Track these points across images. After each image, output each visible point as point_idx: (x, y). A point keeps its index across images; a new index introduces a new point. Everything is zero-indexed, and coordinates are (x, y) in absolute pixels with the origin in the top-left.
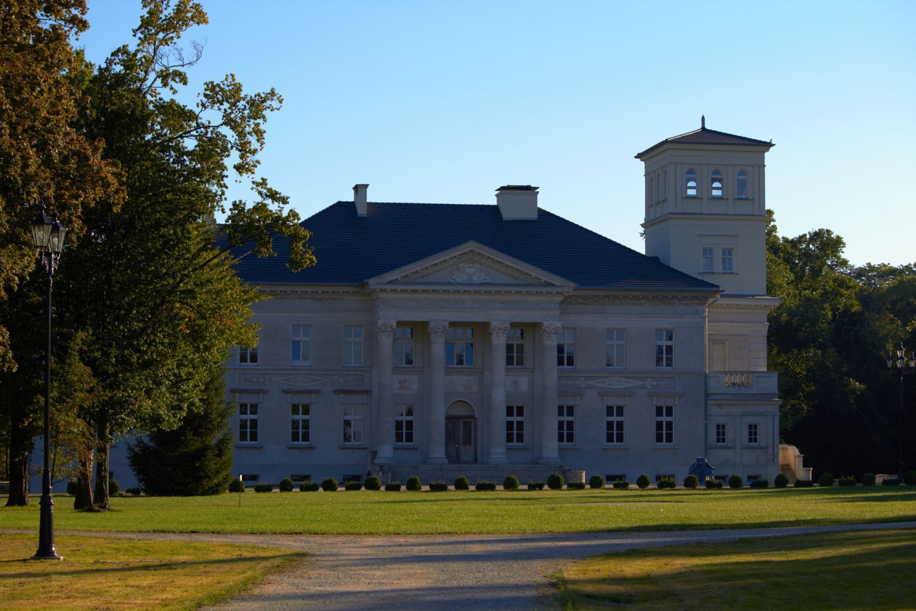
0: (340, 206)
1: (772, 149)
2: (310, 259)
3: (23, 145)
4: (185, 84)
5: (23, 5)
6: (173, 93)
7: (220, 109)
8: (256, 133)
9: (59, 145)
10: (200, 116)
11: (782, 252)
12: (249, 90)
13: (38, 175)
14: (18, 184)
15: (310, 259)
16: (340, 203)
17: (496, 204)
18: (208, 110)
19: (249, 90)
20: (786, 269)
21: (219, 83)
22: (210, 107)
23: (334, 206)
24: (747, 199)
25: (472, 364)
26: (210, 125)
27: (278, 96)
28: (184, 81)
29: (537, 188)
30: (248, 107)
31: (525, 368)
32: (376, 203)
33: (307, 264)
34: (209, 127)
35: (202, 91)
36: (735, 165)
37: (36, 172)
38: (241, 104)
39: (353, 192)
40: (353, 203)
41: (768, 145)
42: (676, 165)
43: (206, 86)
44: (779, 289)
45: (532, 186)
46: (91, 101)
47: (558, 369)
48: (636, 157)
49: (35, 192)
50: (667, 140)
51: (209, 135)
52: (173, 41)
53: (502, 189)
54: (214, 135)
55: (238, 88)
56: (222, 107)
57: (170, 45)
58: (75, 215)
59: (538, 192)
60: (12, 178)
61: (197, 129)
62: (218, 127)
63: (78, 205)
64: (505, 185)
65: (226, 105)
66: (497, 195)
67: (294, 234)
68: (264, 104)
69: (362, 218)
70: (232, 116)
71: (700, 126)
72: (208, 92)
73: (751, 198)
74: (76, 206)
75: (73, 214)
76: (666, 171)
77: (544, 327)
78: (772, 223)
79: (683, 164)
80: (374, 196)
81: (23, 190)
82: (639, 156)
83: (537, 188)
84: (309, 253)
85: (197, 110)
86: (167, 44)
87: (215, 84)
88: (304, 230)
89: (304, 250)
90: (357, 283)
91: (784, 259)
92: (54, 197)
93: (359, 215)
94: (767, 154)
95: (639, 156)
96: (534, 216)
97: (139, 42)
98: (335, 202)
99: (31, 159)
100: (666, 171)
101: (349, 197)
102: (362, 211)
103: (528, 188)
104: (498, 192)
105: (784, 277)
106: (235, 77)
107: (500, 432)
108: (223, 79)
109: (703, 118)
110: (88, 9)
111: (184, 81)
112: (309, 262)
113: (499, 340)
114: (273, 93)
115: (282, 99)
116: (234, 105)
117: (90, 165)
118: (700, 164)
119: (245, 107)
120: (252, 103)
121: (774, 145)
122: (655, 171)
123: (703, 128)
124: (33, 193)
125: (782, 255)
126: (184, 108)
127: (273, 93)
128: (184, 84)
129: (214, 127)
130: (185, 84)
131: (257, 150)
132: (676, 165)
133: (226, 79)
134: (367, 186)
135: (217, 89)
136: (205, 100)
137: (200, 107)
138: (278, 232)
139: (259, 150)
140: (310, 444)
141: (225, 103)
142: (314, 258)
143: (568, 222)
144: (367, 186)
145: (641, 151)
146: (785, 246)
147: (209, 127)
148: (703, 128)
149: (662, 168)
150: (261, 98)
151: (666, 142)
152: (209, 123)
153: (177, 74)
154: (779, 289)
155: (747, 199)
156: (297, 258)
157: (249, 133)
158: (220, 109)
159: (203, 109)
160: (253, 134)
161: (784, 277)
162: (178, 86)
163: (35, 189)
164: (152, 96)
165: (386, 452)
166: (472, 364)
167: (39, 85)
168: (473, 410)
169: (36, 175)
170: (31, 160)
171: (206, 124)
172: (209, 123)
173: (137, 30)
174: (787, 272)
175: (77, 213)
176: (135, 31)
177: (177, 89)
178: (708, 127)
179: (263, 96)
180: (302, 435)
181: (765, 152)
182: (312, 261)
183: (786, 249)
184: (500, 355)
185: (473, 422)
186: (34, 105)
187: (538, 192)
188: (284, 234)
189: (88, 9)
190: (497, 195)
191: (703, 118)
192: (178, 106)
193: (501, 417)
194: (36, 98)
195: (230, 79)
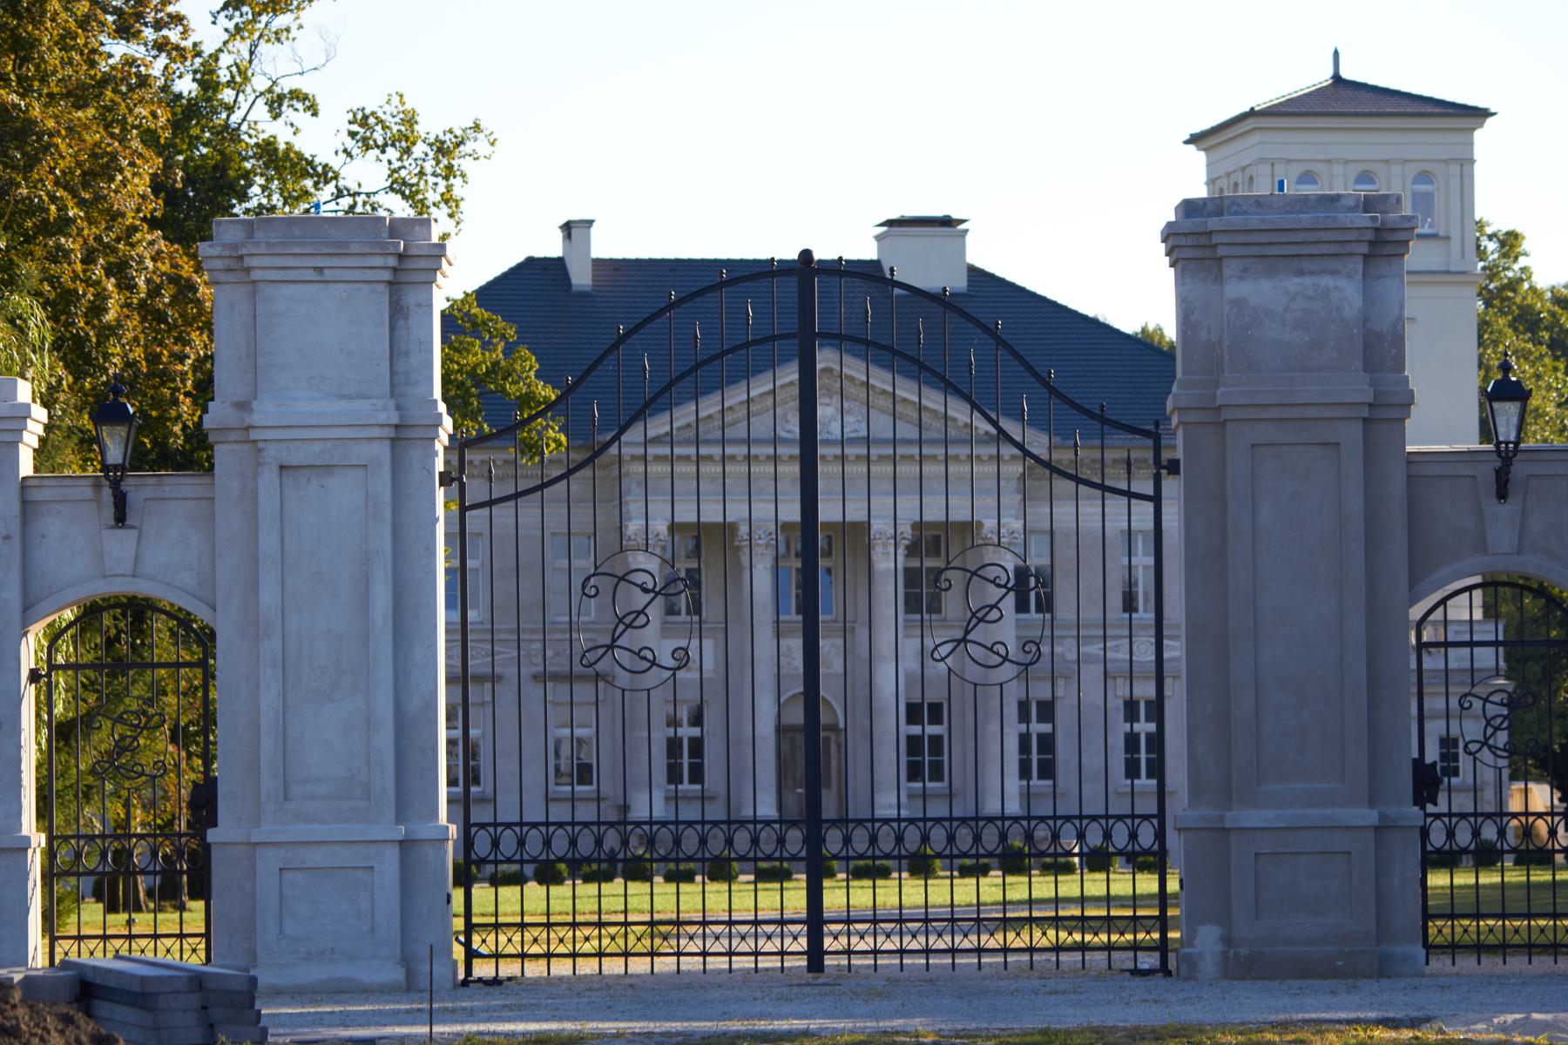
0: (531, 266)
1: (1489, 121)
2: (555, 440)
3: (95, 274)
4: (315, 114)
5: (88, 31)
6: (295, 134)
7: (379, 160)
8: (446, 202)
9: (147, 268)
10: (343, 173)
11: (1546, 329)
12: (430, 126)
13: (122, 326)
14: (90, 341)
15: (555, 440)
16: (530, 262)
17: (875, 257)
18: (358, 161)
19: (430, 126)
20: (1556, 369)
21: (375, 109)
22: (360, 156)
23: (519, 267)
24: (1434, 236)
25: (831, 613)
26: (361, 190)
27: (488, 133)
28: (313, 110)
29: (962, 221)
30: (431, 154)
31: (945, 620)
32: (611, 261)
33: (551, 448)
34: (359, 194)
35: (346, 127)
36: (1406, 161)
37: (118, 320)
38: (419, 149)
39: (559, 235)
40: (560, 260)
41: (1482, 114)
42: (1273, 165)
43: (351, 115)
44: (1536, 419)
45: (955, 216)
46: (182, 178)
47: (1017, 620)
48: (1187, 142)
49: (118, 355)
50: (1252, 109)
51: (359, 209)
52: (291, 36)
53: (890, 223)
54: (368, 208)
55: (410, 120)
56: (384, 157)
57: (285, 42)
58: (182, 391)
59: (966, 231)
60: (82, 334)
61: (337, 197)
62: (374, 193)
63: (186, 373)
64: (895, 216)
65: (392, 153)
66: (879, 238)
67: (526, 394)
68: (462, 148)
69: (583, 295)
70: (403, 173)
71: (1330, 73)
72: (355, 128)
73: (1442, 233)
74: (183, 374)
75: (178, 389)
76: (1251, 178)
77: (984, 531)
78: (1522, 261)
79: (1289, 161)
80: (607, 244)
81: (97, 352)
82: (1195, 139)
83: (962, 221)
84: (553, 428)
85: (336, 162)
86: (278, 40)
87: (367, 112)
88: (544, 386)
89: (544, 423)
90: (581, 442)
91: (1553, 345)
92: (146, 359)
93: (574, 288)
94: (1478, 134)
95: (1195, 139)
96: (959, 283)
97: (226, 36)
98: (520, 259)
99: (111, 298)
100: (1251, 178)
101: (553, 247)
102: (581, 278)
103: (947, 222)
104: (884, 229)
105: (1549, 388)
106: (405, 99)
107: (889, 760)
108: (383, 101)
109: (1336, 54)
110: (194, 31)
111: (313, 110)
112: (553, 445)
113: (887, 561)
114: (477, 127)
115: (495, 140)
116: (407, 151)
117: (198, 300)
118: (1329, 161)
119: (426, 155)
120: (441, 149)
121: (1495, 114)
122: (1228, 175)
123: (1337, 78)
124: (113, 355)
125: (1546, 335)
126: (313, 161)
127: (477, 127)
128: (313, 115)
129: (368, 195)
130: (315, 114)
131: (449, 234)
132: (1273, 165)
133: (388, 102)
134: (590, 223)
135: (372, 121)
136: (350, 143)
137: (343, 156)
138: (496, 391)
139: (453, 235)
140: (483, 792)
141: (390, 150)
142: (563, 438)
143: (1033, 295)
144: (590, 223)
145: (1197, 129)
146: (1553, 314)
147: (359, 194)
148: (1337, 78)
149: (1243, 169)
150: (456, 137)
151: (1252, 113)
152: (359, 185)
153: (296, 95)
154: (1536, 419)
155: (1434, 236)
156: (531, 439)
157: (434, 204)
158: (379, 160)
159: (349, 159)
160: (442, 205)
161: (1549, 388)
162: (301, 117)
163: (118, 350)
164: (250, 137)
165: (650, 803)
166: (831, 613)
167: (121, 171)
168: (834, 711)
169: (119, 326)
170: (112, 301)
171: (354, 188)
172: (359, 185)
173: (218, 12)
174: (1557, 378)
175: (185, 386)
176: (215, 16)
177: (299, 127)
178: (1346, 74)
179: (459, 133)
180: (681, 753)
181: (1474, 129)
182: (558, 443)
183: (1559, 320)
184: (888, 594)
185: (833, 739)
186: (116, 207)
187: (966, 231)
188: (509, 394)
189: (194, 31)
190: (879, 238)
191: (1336, 54)
192: (300, 156)
193: (891, 728)
194: (116, 192)
195: (395, 100)
